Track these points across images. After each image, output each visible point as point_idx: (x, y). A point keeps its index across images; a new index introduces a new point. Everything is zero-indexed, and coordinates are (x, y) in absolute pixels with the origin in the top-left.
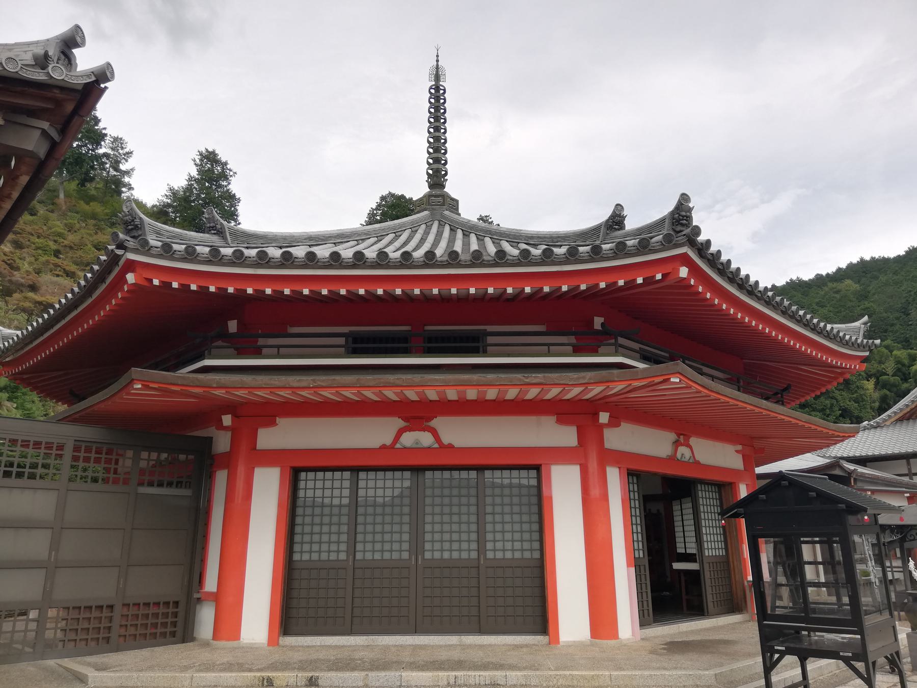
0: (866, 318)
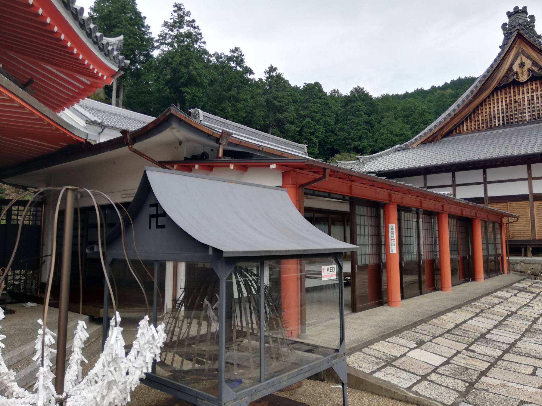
0: (122, 37)
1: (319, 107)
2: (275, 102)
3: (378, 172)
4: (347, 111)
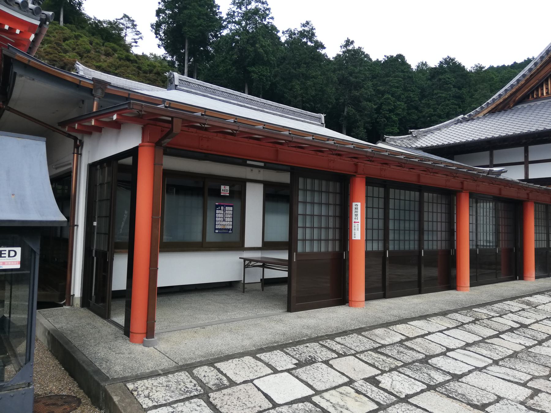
1: (400, 81)
2: (351, 78)
3: (431, 147)
4: (433, 84)
